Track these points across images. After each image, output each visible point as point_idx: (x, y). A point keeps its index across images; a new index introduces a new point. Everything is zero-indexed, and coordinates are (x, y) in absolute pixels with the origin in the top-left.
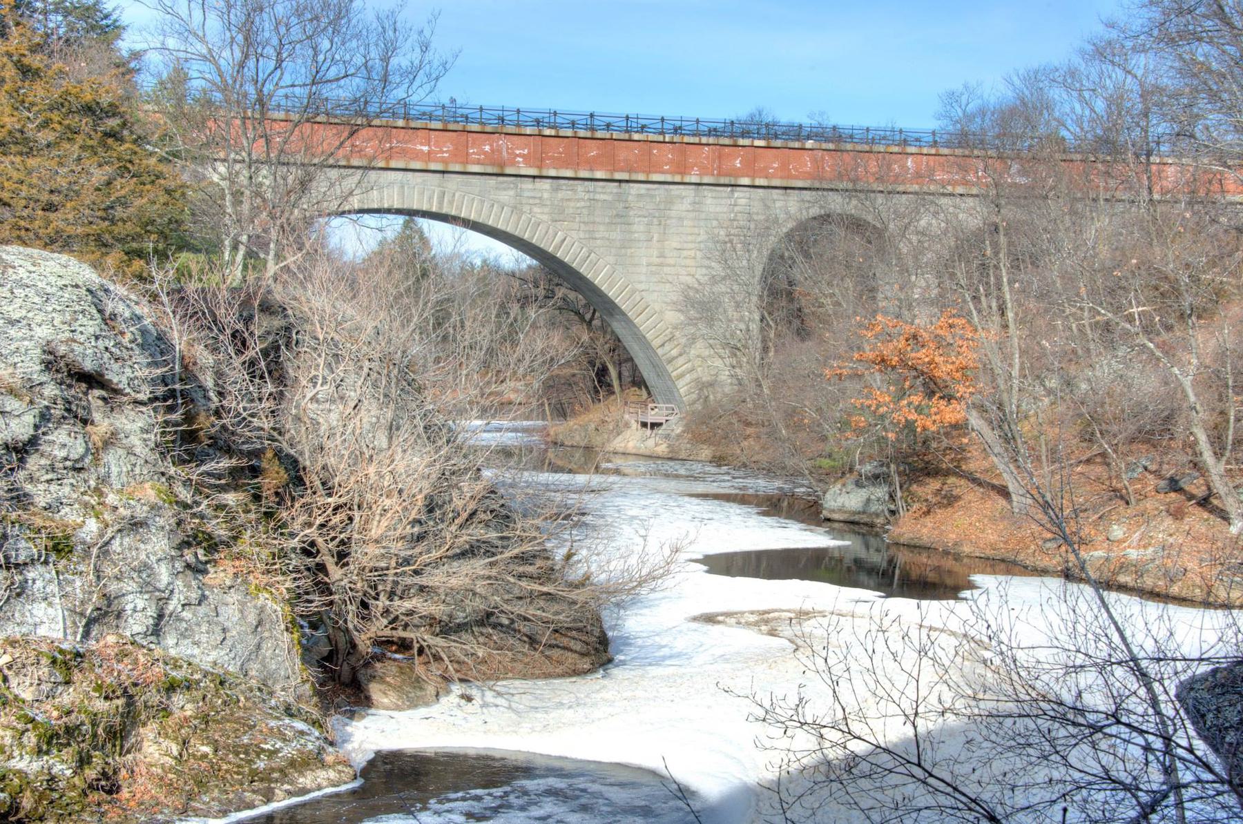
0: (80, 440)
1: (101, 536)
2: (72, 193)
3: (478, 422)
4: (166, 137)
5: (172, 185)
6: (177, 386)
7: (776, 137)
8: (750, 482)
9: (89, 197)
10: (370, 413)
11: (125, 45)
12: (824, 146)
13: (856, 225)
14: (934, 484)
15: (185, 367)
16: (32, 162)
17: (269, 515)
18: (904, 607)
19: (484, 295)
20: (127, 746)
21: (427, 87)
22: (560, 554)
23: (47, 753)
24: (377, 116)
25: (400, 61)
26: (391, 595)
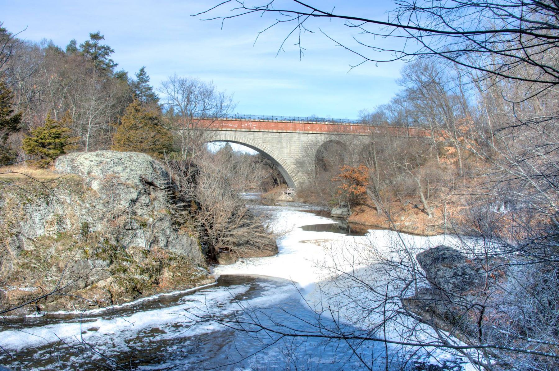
0: (148, 199)
1: (153, 222)
2: (146, 139)
3: (244, 193)
4: (168, 124)
5: (169, 136)
6: (171, 185)
7: (318, 121)
8: (313, 207)
9: (150, 139)
10: (218, 191)
11: (160, 102)
12: (330, 123)
13: (338, 143)
14: (359, 207)
15: (173, 180)
16: (137, 132)
17: (193, 217)
18: (351, 237)
19: (246, 161)
20: (161, 273)
21: (231, 110)
22: (265, 226)
23: (143, 274)
24: (219, 118)
25: (225, 104)
26: (224, 237)
